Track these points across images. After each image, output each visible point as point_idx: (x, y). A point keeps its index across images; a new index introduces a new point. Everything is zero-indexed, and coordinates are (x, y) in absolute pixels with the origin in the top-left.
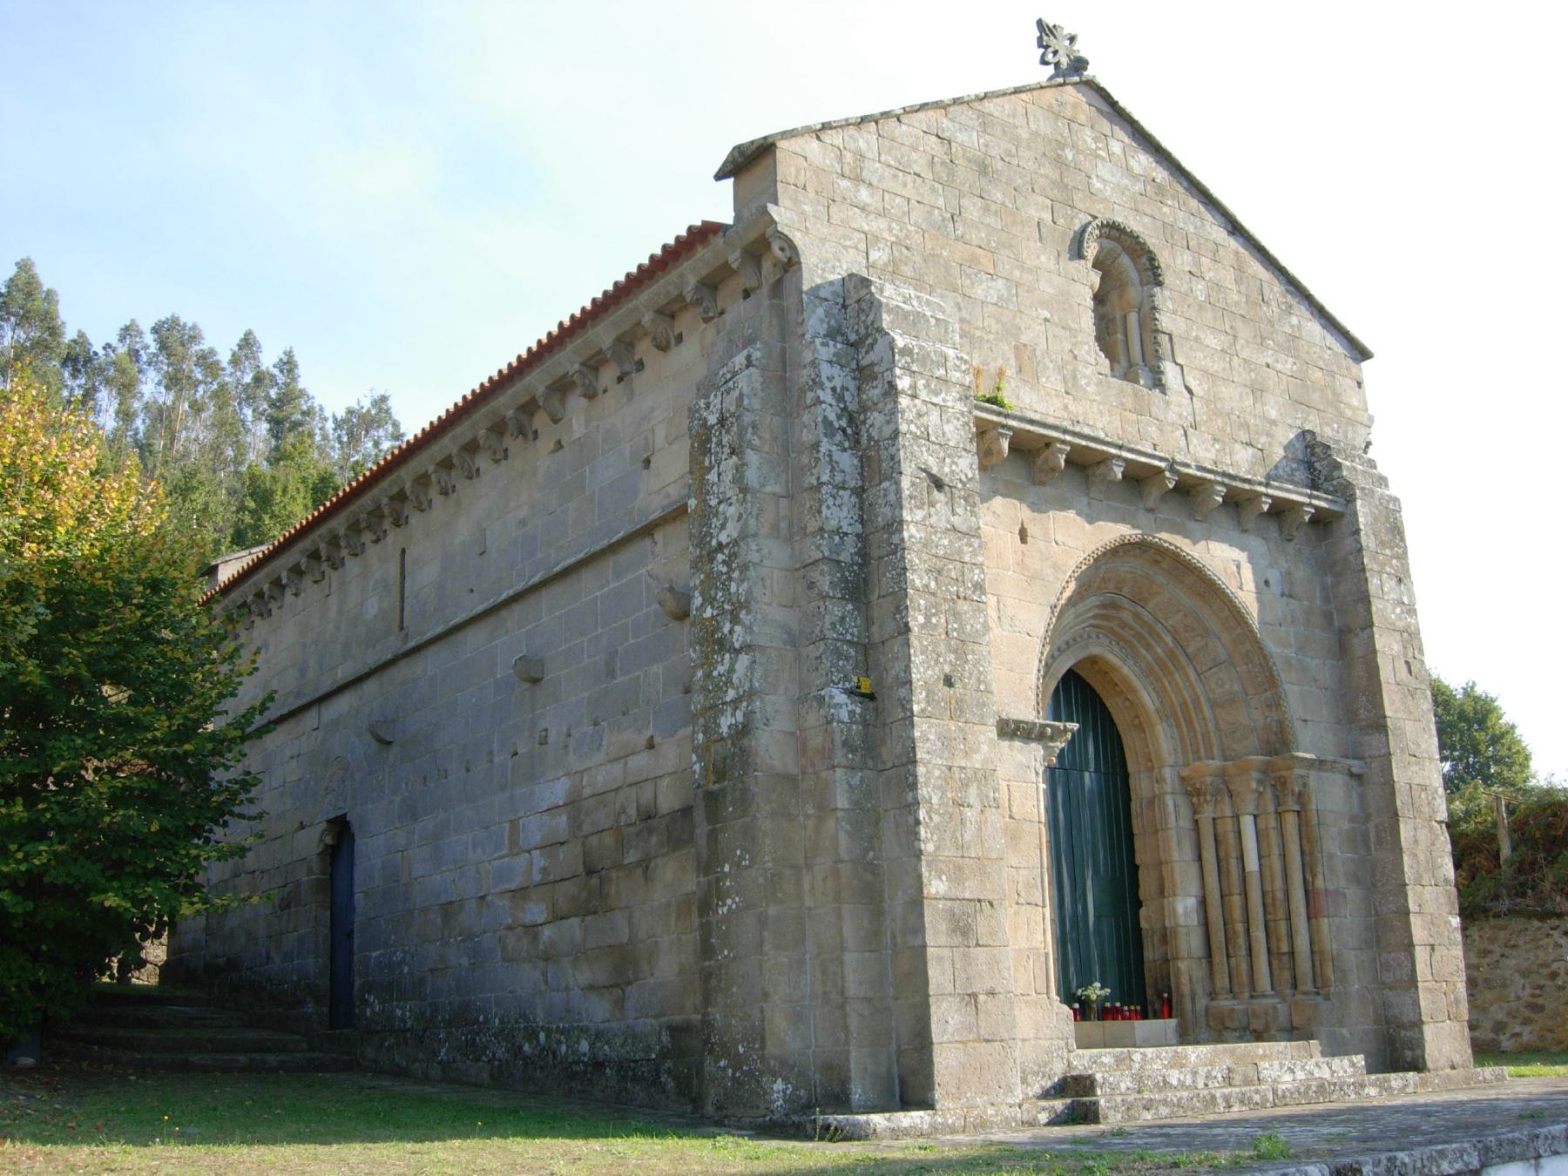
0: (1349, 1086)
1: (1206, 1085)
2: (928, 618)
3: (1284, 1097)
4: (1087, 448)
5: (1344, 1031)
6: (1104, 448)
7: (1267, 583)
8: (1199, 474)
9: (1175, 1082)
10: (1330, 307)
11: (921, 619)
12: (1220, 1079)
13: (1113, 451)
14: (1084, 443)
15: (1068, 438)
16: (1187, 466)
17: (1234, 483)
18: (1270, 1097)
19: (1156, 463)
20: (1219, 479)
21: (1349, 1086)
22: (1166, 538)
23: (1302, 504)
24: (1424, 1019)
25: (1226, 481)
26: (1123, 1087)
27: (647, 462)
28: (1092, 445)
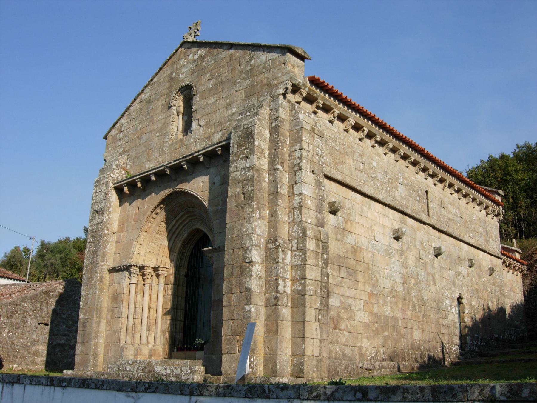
0: (164, 376)
1: (137, 371)
2: (89, 249)
3: (140, 377)
4: (143, 176)
6: (147, 174)
7: (214, 183)
8: (175, 163)
9: (128, 369)
10: (269, 43)
11: (88, 250)
12: (141, 370)
13: (149, 173)
15: (138, 177)
16: (170, 163)
18: (136, 376)
19: (161, 168)
20: (181, 160)
21: (164, 376)
23: (215, 148)
24: (223, 352)
25: (184, 159)
26: (115, 369)
28: (143, 175)
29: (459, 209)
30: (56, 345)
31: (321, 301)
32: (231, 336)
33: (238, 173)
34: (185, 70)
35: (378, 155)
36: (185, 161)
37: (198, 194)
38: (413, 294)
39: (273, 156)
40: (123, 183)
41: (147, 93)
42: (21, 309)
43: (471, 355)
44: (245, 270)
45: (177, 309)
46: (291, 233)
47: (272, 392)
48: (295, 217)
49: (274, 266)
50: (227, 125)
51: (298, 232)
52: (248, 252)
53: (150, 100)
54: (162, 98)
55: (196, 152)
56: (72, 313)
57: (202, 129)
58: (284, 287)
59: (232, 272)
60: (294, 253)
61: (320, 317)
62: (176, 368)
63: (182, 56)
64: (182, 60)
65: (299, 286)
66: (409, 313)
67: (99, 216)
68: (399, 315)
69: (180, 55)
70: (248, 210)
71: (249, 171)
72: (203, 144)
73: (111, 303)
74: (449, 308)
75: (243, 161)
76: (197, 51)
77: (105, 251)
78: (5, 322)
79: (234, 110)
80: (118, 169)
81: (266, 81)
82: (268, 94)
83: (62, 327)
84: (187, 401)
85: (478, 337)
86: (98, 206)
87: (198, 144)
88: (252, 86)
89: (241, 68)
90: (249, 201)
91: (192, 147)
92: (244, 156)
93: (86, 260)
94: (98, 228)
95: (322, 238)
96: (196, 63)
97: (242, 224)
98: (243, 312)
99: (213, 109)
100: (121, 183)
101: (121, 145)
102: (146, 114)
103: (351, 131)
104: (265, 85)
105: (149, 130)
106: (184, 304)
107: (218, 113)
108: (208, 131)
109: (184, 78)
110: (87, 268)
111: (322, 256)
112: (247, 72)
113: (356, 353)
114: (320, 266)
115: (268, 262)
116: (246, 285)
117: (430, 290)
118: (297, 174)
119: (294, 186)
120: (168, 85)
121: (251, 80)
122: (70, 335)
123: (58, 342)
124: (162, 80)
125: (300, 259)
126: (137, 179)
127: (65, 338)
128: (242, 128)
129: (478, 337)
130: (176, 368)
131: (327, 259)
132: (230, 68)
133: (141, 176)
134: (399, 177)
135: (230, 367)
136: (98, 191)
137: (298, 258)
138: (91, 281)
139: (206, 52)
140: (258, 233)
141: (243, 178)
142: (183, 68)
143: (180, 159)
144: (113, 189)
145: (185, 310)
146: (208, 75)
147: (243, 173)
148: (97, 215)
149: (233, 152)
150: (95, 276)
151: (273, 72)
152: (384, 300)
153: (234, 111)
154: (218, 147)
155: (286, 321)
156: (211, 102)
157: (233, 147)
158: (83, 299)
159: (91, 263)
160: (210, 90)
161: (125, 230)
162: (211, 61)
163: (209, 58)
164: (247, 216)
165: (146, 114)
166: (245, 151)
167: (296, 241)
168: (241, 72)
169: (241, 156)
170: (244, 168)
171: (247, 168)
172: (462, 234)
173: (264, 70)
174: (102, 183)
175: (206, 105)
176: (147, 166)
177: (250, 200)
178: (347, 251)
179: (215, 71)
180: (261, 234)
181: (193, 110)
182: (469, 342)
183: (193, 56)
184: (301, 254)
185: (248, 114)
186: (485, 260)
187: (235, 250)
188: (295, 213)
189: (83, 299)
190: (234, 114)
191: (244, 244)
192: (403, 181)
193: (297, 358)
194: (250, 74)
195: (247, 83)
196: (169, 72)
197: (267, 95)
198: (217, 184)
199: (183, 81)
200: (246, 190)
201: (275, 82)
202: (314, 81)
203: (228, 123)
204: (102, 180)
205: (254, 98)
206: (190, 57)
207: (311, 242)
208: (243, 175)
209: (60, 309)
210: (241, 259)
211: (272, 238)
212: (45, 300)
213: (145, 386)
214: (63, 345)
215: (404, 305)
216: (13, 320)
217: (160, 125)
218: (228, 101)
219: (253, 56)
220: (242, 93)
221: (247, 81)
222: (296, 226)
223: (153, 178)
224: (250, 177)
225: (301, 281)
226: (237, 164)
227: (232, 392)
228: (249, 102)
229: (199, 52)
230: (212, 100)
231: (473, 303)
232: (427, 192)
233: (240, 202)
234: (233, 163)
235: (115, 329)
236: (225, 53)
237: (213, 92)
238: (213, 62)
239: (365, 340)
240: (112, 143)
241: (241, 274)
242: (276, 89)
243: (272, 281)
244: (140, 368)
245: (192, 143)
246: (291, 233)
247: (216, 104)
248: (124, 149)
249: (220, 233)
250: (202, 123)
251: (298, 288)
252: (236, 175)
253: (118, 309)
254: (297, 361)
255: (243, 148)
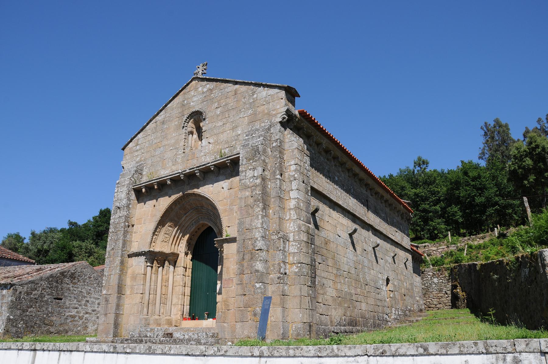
2: (111, 237)
3: (162, 341)
5: (225, 324)
6: (164, 179)
9: (148, 336)
11: (110, 238)
13: (166, 178)
14: (159, 180)
15: (155, 181)
16: (186, 171)
17: (200, 168)
22: (190, 192)
25: (197, 169)
27: (154, 206)
29: (385, 213)
30: (68, 316)
31: (311, 280)
32: (244, 308)
33: (248, 180)
34: (195, 99)
35: (339, 172)
36: (198, 170)
37: (209, 196)
38: (361, 276)
39: (274, 169)
40: (141, 185)
41: (161, 115)
42: (39, 287)
43: (395, 322)
44: (255, 256)
45: (185, 286)
46: (289, 228)
47: (340, 351)
48: (292, 215)
49: (277, 253)
50: (233, 143)
51: (294, 227)
52: (257, 242)
53: (164, 121)
54: (175, 120)
55: (209, 163)
56: (82, 290)
57: (211, 145)
58: (285, 269)
59: (243, 258)
60: (291, 243)
61: (311, 292)
62: (193, 334)
63: (192, 88)
64: (193, 91)
65: (296, 269)
66: (359, 290)
67: (120, 211)
68: (353, 291)
69: (191, 87)
70: (257, 209)
71: (256, 179)
72: (212, 157)
73: (131, 282)
74: (382, 286)
75: (251, 172)
76: (206, 85)
77: (125, 239)
78: (25, 298)
79: (239, 132)
80: (137, 174)
81: (266, 111)
82: (269, 121)
83: (73, 301)
84: (257, 361)
85: (399, 308)
86: (120, 203)
87: (208, 157)
88: (255, 114)
89: (244, 100)
90: (257, 202)
91: (203, 159)
92: (252, 167)
93: (108, 246)
94: (120, 221)
95: (311, 233)
96: (205, 95)
97: (251, 220)
98: (254, 289)
99: (221, 130)
100: (140, 186)
101: (138, 155)
102: (160, 132)
103: (323, 153)
104: (266, 114)
105: (163, 145)
106: (190, 283)
107: (225, 134)
108: (217, 147)
109: (195, 105)
110: (109, 253)
111: (311, 246)
112: (251, 103)
113: (329, 320)
114: (309, 253)
115: (272, 250)
116: (256, 268)
117: (371, 273)
118: (293, 183)
119: (290, 192)
120: (180, 110)
121: (253, 109)
122: (80, 308)
123: (70, 314)
124: (175, 106)
125: (297, 248)
126: (155, 182)
127: (76, 310)
128: (250, 146)
129: (399, 308)
130: (193, 334)
131: (314, 249)
132: (236, 99)
133: (159, 180)
134: (351, 189)
135: (243, 332)
136: (119, 191)
137: (295, 247)
138: (114, 264)
139: (214, 86)
140: (265, 227)
141: (251, 185)
142: (194, 97)
143: (195, 168)
144: (133, 190)
145: (191, 287)
146: (216, 104)
147: (251, 180)
148: (118, 211)
149: (242, 164)
150: (117, 260)
151: (272, 105)
152: (344, 280)
153: (239, 133)
154: (228, 160)
155: (287, 295)
156: (219, 125)
157: (243, 160)
158: (106, 278)
159: (113, 249)
160: (218, 116)
161: (143, 223)
162: (218, 94)
163: (216, 91)
164: (256, 214)
165: (160, 132)
166: (253, 164)
167: (292, 234)
168: (244, 103)
169: (250, 168)
170: (252, 177)
171: (255, 176)
172: (388, 233)
173: (264, 103)
174: (123, 184)
175: (214, 127)
176: (162, 173)
177: (258, 201)
178: (321, 243)
179: (222, 101)
180: (267, 228)
181: (203, 131)
182: (394, 312)
183: (202, 89)
184: (297, 244)
185: (254, 135)
186: (402, 254)
187: (245, 240)
188: (291, 212)
189: (106, 278)
190: (239, 135)
191: (254, 235)
192: (353, 192)
193: (296, 324)
194: (252, 105)
195: (250, 112)
196: (181, 100)
197: (268, 122)
198: (225, 189)
199: (194, 107)
200: (254, 193)
201: (274, 113)
202: (302, 113)
203: (234, 142)
204: (123, 182)
205: (256, 124)
206: (200, 89)
207: (305, 235)
208: (251, 182)
209: (72, 287)
210: (251, 247)
211: (275, 232)
212: (60, 279)
213: (214, 350)
214: (73, 317)
215: (356, 284)
216: (32, 296)
217: (173, 141)
218: (234, 124)
219: (255, 91)
220: (246, 119)
221: (250, 110)
222: (292, 223)
223: (169, 182)
224: (257, 184)
225: (298, 265)
226: (246, 173)
227: (302, 352)
228: (252, 127)
229: (208, 86)
230: (220, 123)
231: (395, 283)
232: (367, 201)
233: (249, 203)
234: (243, 173)
235: (134, 303)
236: (231, 87)
237: (220, 118)
238: (220, 94)
239: (333, 310)
240: (130, 153)
241: (252, 259)
242: (275, 118)
243: (275, 264)
244: (159, 334)
245: (203, 156)
246: (289, 228)
247: (224, 126)
248: (140, 159)
249: (229, 227)
250: (211, 141)
251: (295, 270)
252: (245, 182)
253: (136, 286)
254: (296, 327)
255: (251, 161)
